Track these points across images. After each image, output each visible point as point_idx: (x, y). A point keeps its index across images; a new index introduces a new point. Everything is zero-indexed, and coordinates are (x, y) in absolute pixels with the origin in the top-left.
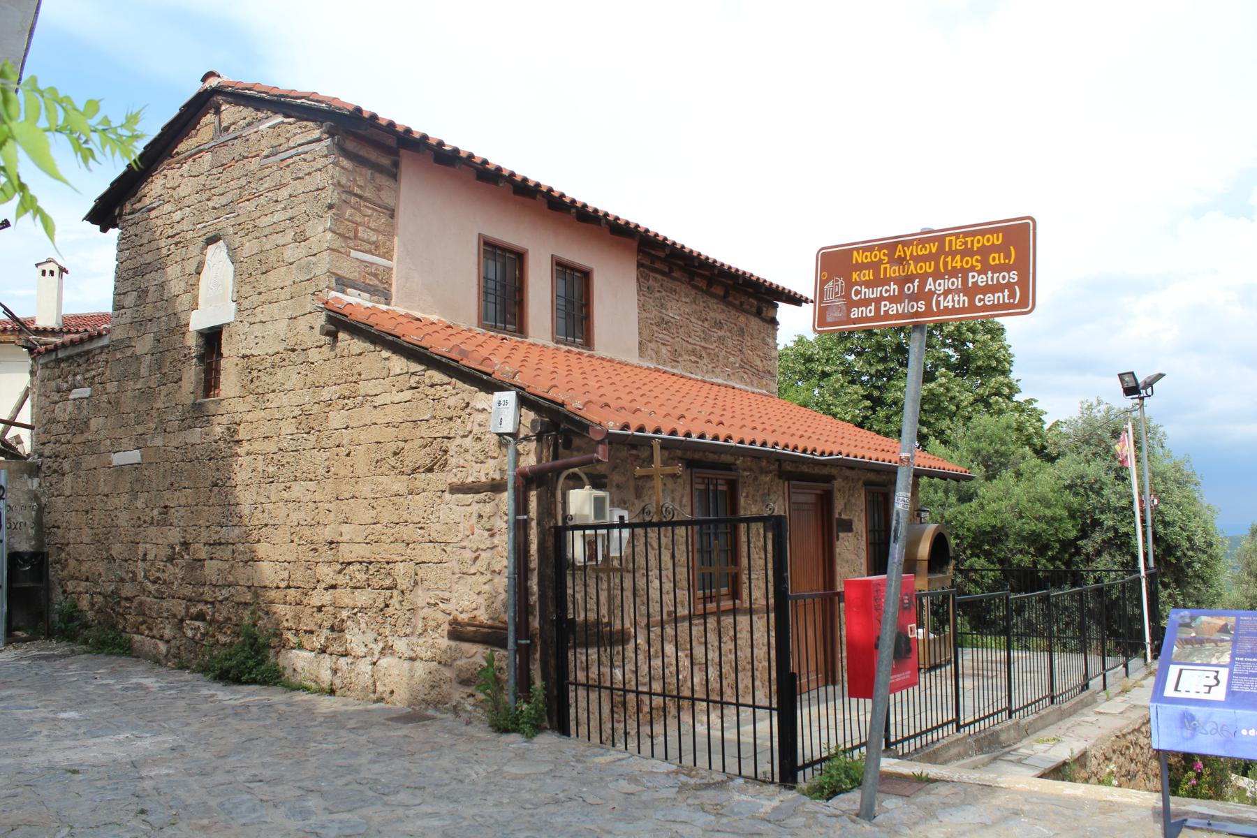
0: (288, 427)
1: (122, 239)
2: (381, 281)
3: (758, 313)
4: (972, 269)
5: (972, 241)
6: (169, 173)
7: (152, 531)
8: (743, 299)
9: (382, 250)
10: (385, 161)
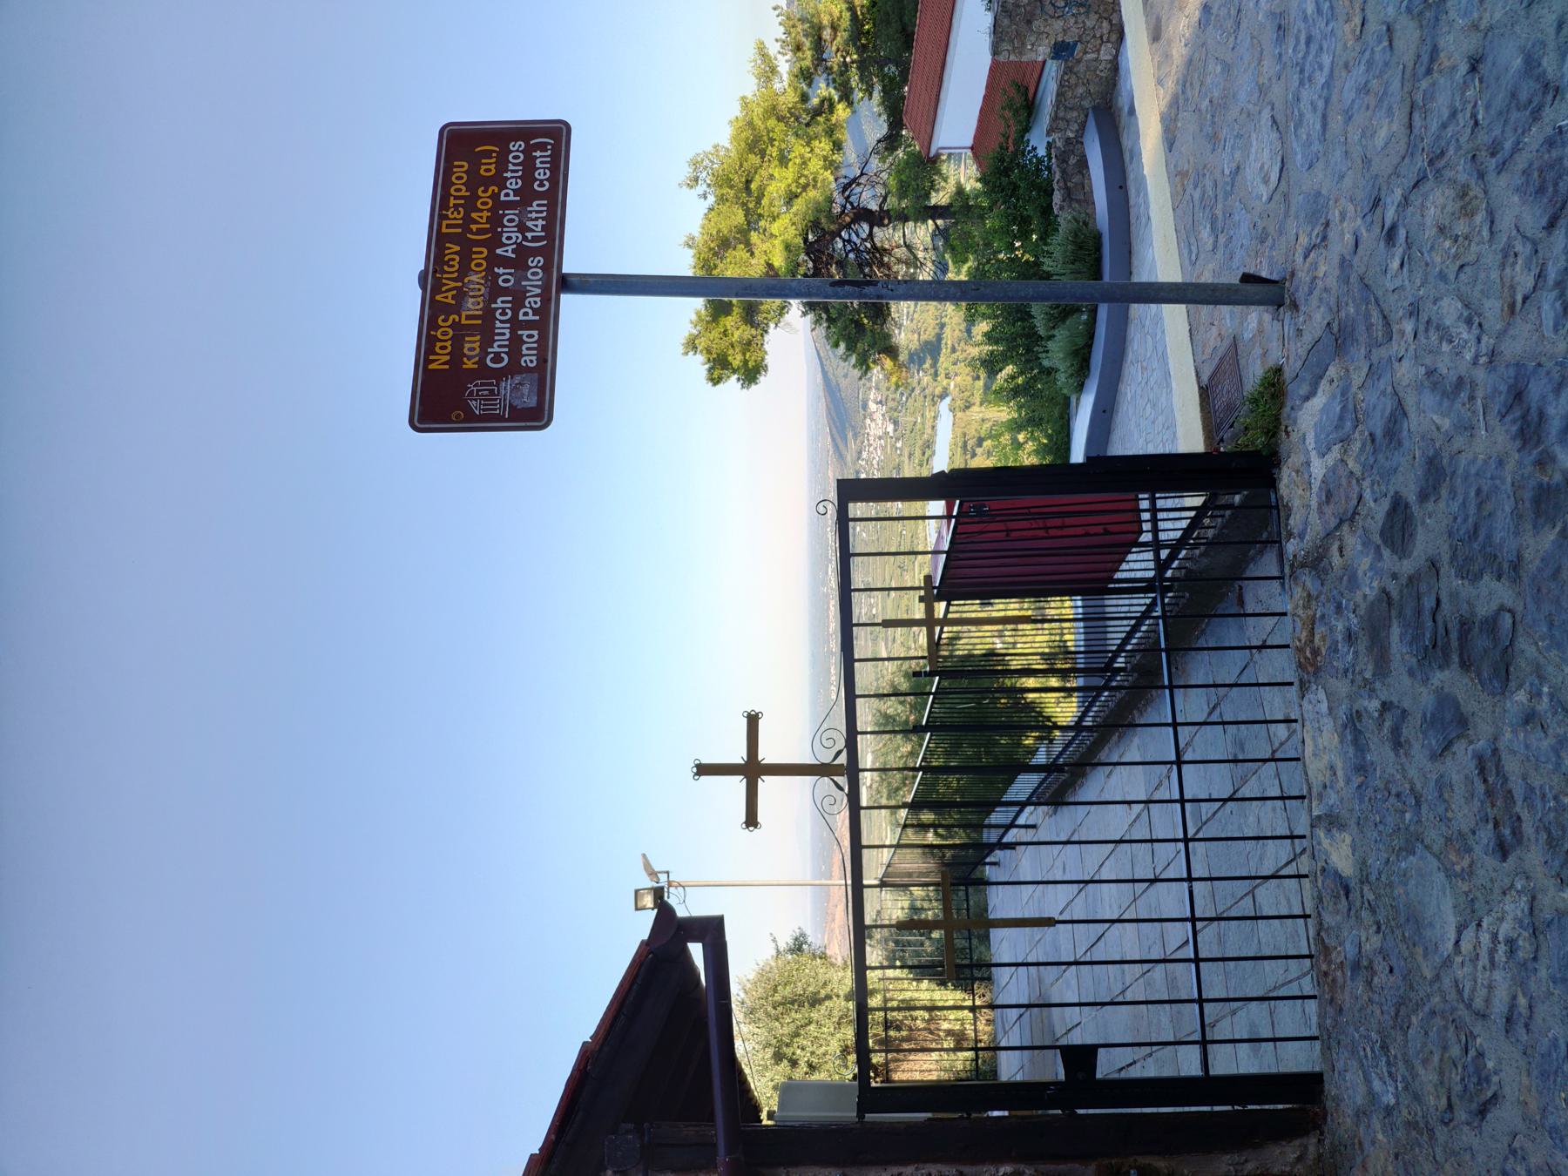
4: (495, 197)
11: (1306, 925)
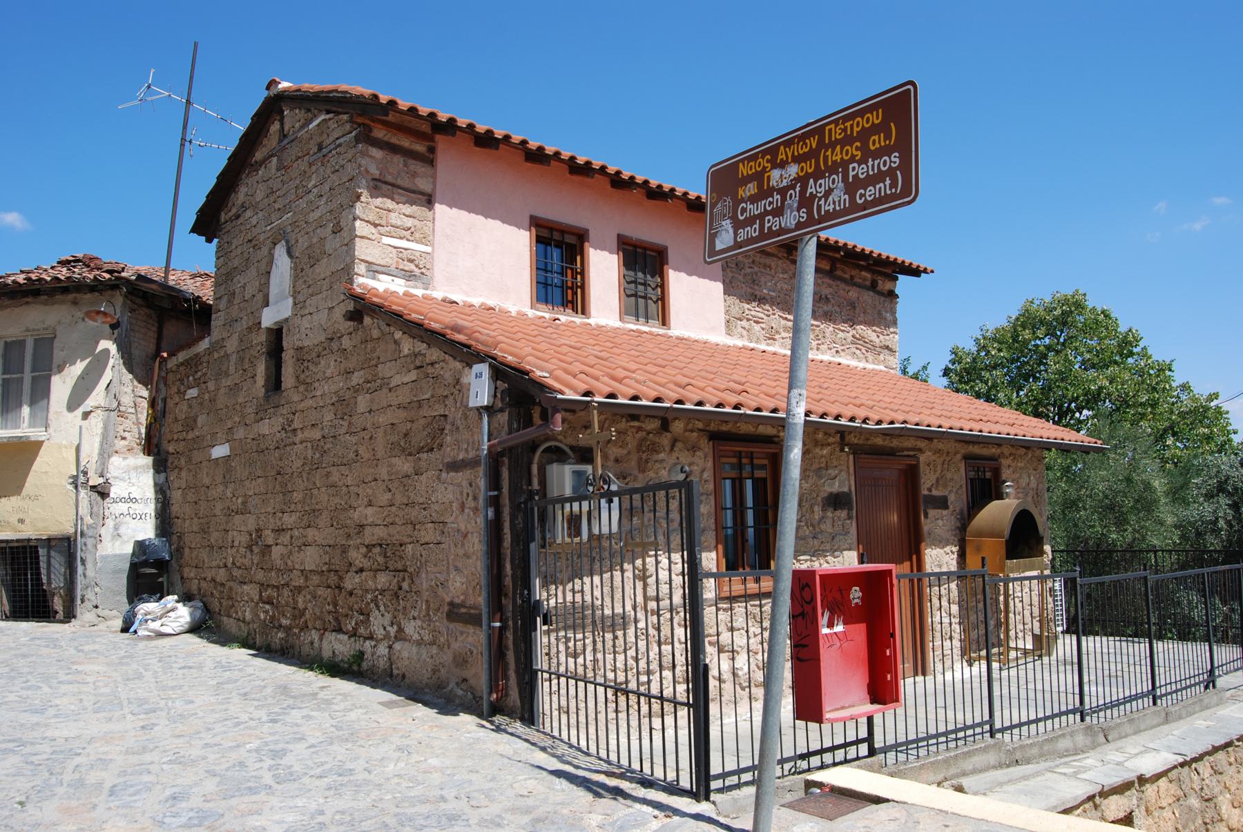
0: (328, 416)
1: (219, 247)
2: (417, 266)
3: (873, 287)
4: (852, 159)
5: (852, 126)
6: (250, 180)
7: (237, 519)
8: (854, 272)
9: (417, 235)
10: (420, 148)
11: (1135, 697)
